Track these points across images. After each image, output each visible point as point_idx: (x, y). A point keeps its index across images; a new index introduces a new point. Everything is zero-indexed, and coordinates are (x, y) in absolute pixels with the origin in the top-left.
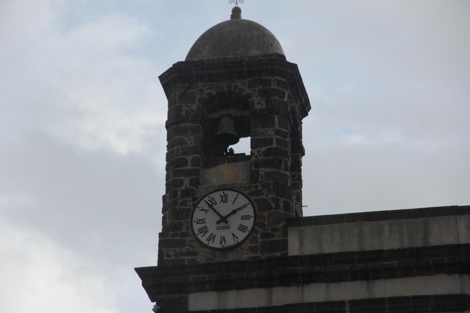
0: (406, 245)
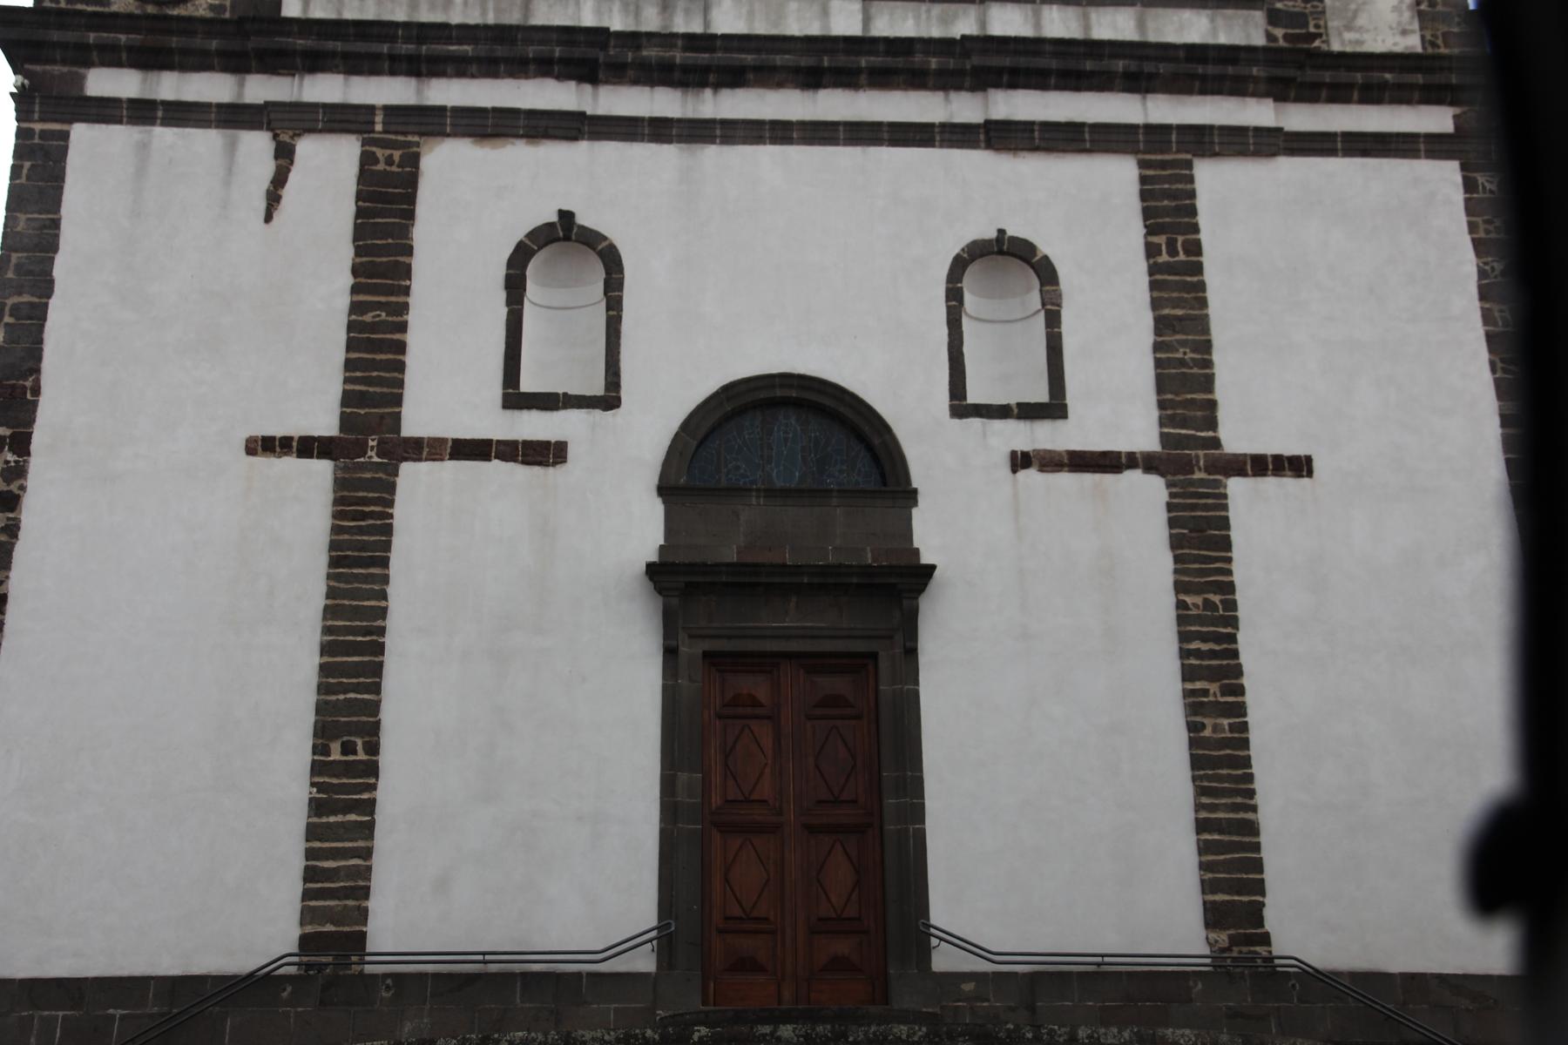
0: (491, 19)
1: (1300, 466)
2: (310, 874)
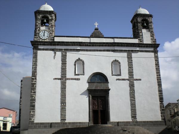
1: (140, 80)
2: (61, 114)
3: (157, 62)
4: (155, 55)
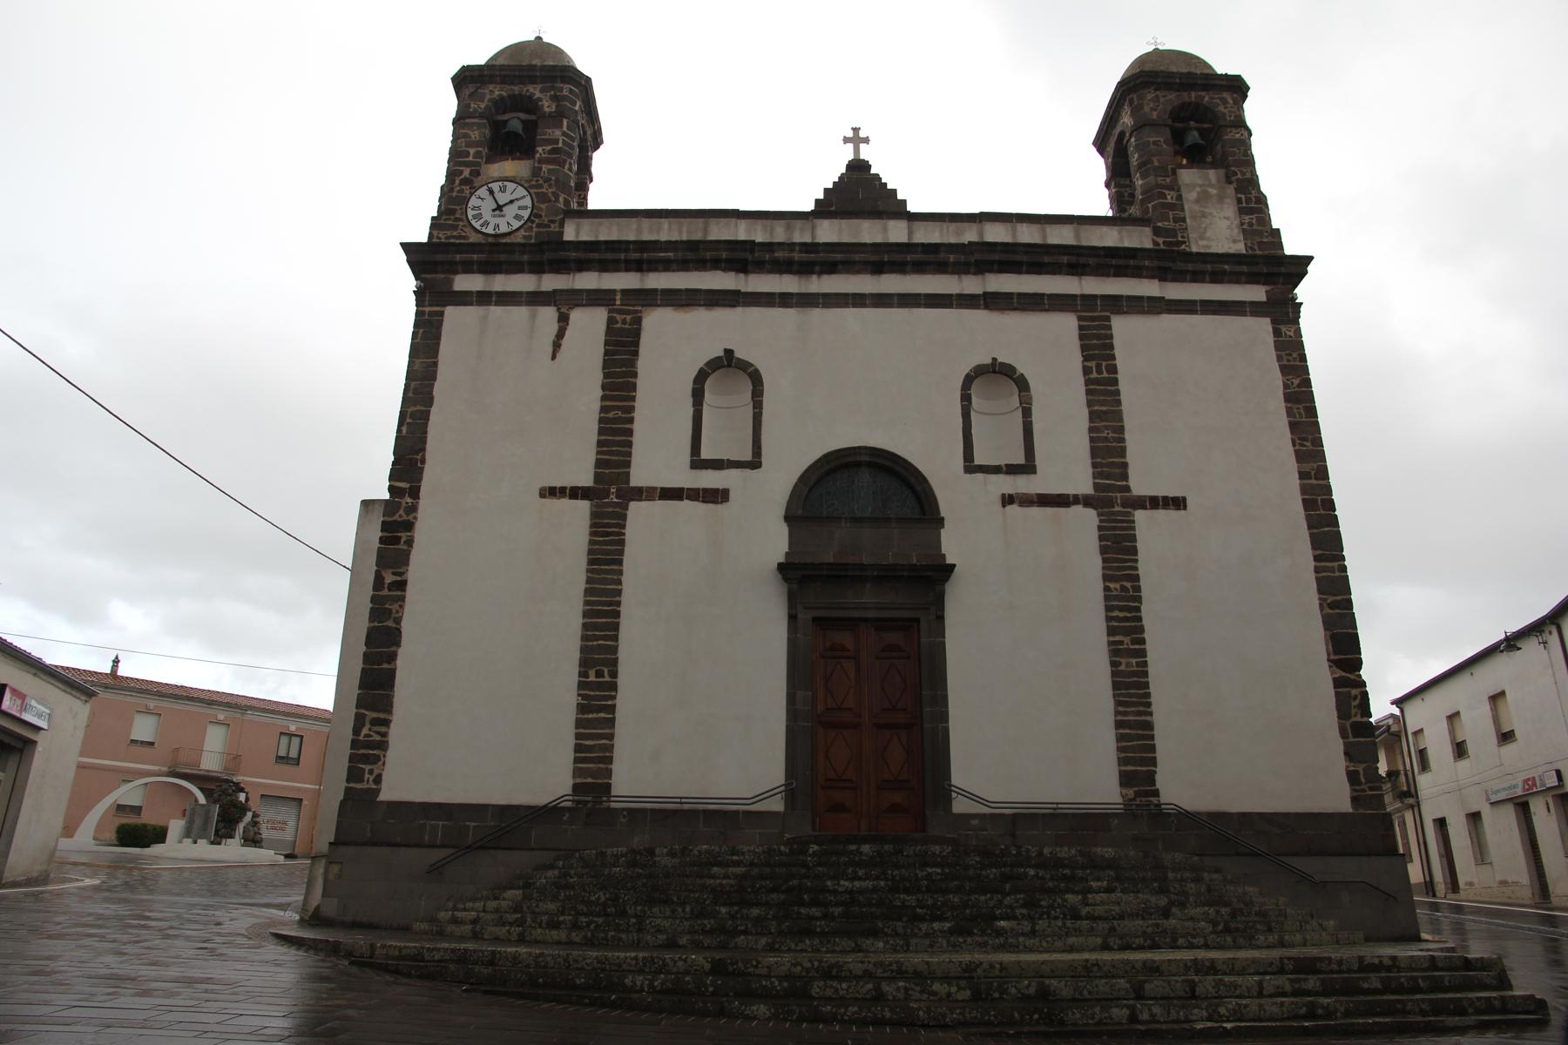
1: (1178, 503)
3: (1296, 382)
4: (1277, 333)
